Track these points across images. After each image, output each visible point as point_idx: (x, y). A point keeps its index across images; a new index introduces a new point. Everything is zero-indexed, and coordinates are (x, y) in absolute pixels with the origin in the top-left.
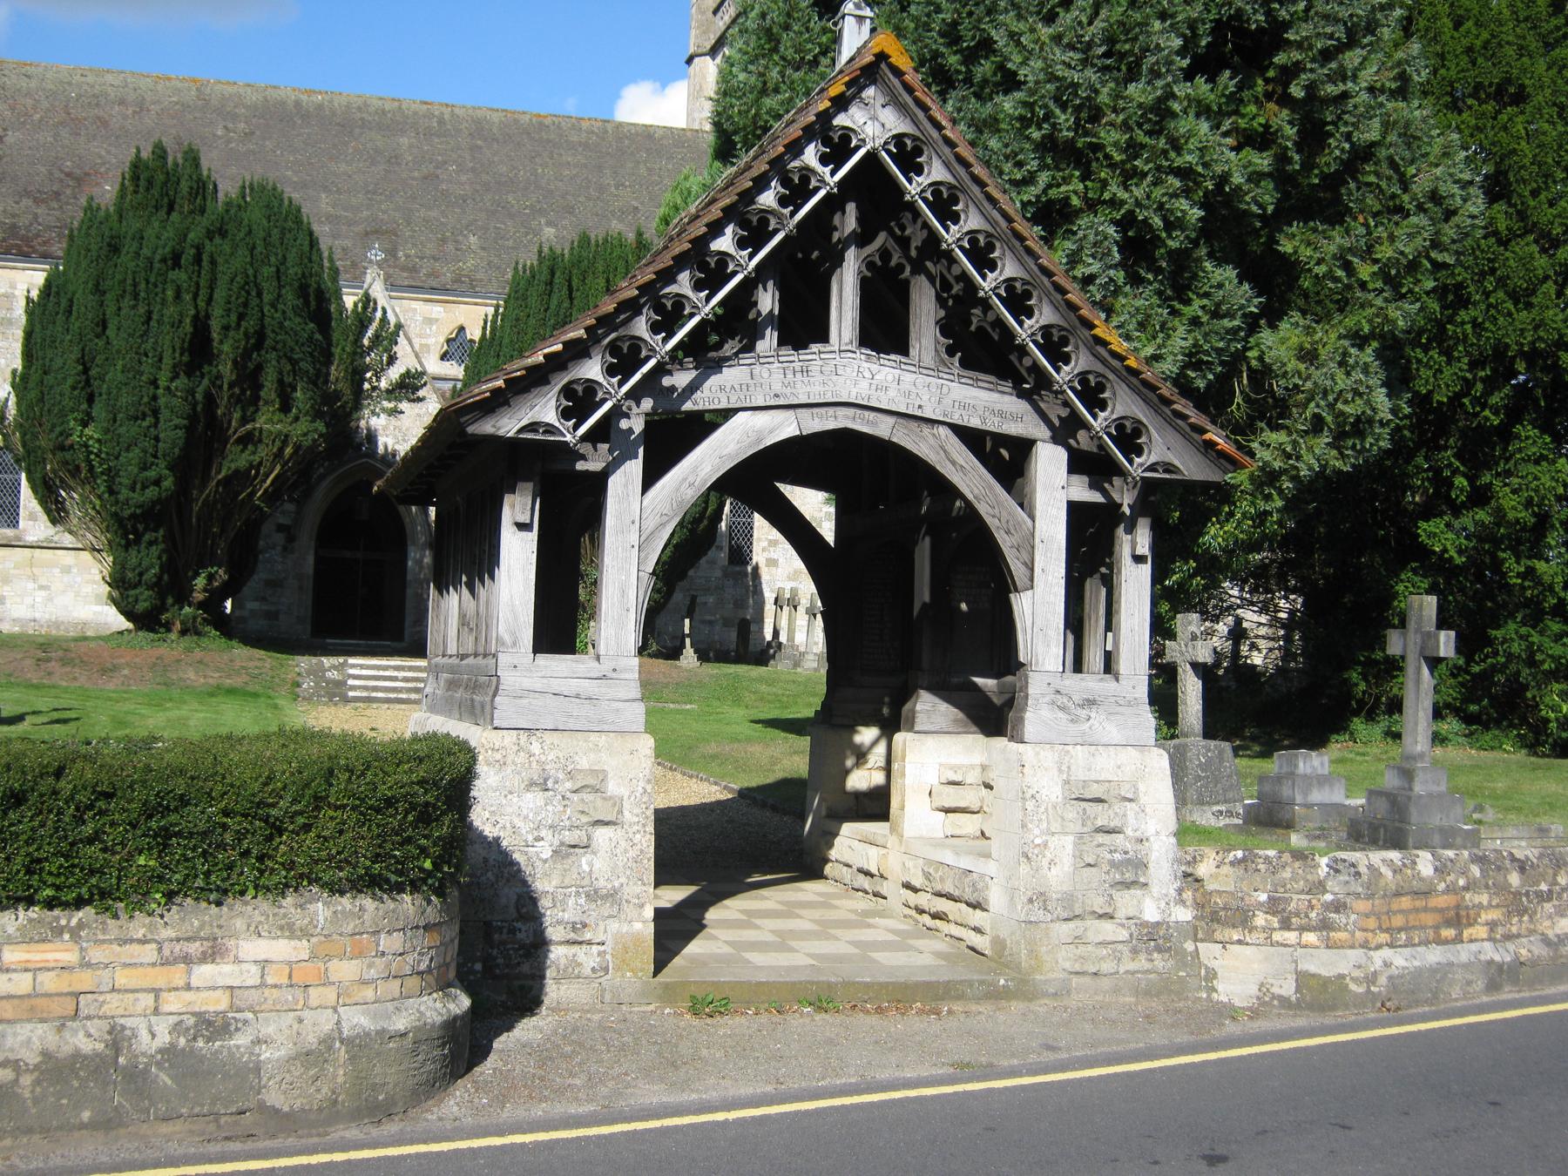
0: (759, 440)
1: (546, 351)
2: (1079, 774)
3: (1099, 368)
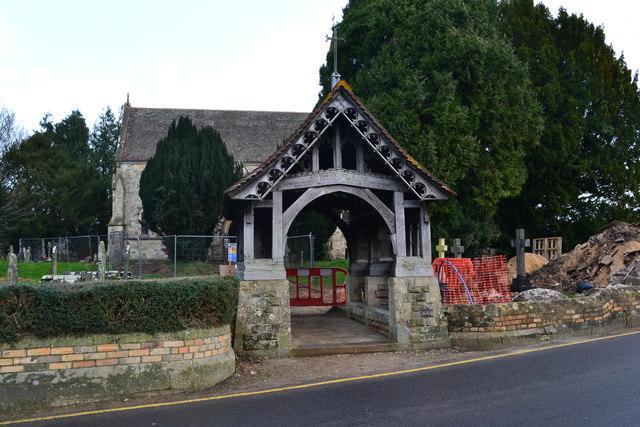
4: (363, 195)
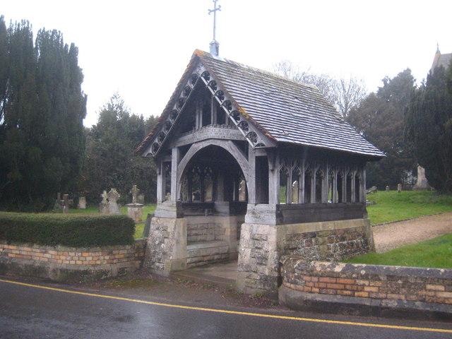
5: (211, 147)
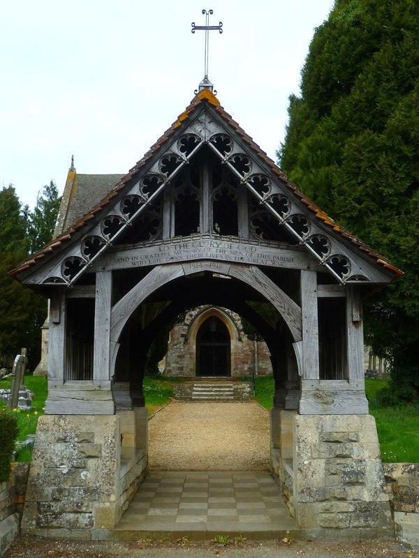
0: (165, 279)
1: (52, 245)
2: (328, 429)
3: (321, 232)
4: (246, 276)
5: (208, 274)
